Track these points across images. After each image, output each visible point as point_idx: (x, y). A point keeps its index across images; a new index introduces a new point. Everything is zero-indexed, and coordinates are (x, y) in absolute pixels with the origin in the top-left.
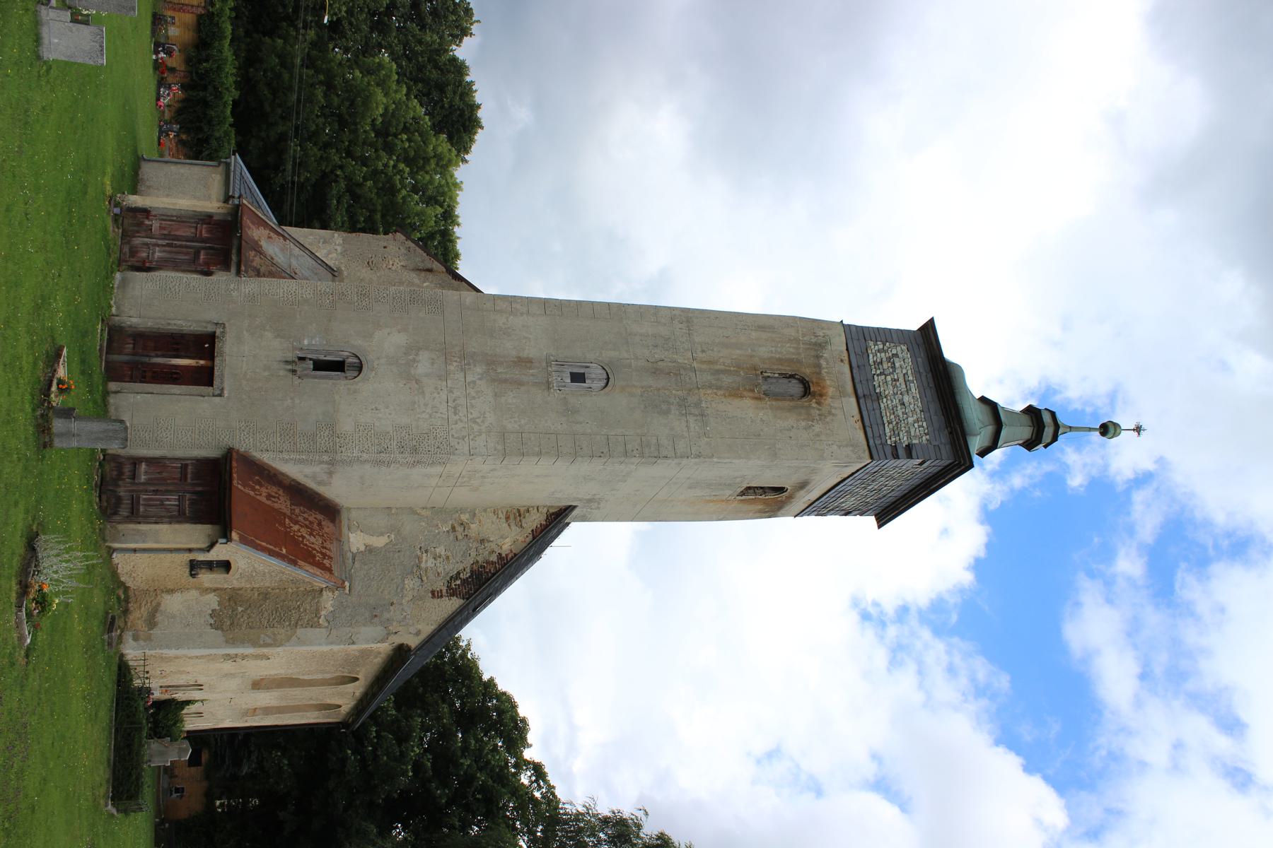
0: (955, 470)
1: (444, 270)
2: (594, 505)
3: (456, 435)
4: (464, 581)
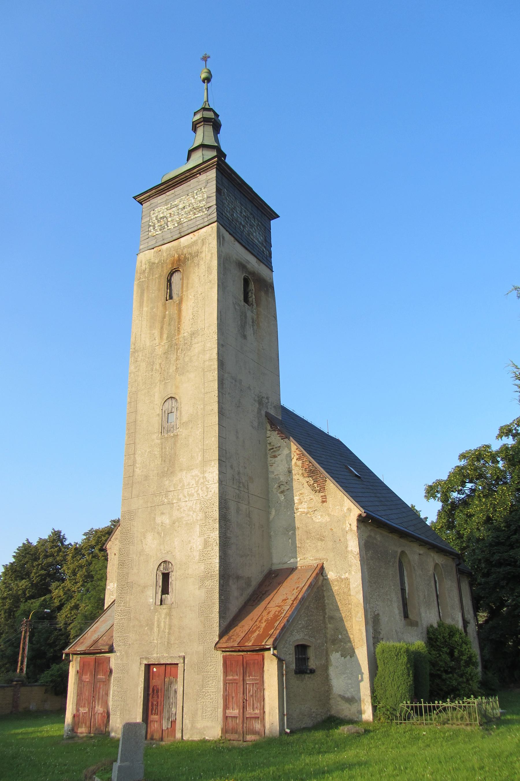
0: (223, 167)
2: (265, 400)
4: (315, 481)
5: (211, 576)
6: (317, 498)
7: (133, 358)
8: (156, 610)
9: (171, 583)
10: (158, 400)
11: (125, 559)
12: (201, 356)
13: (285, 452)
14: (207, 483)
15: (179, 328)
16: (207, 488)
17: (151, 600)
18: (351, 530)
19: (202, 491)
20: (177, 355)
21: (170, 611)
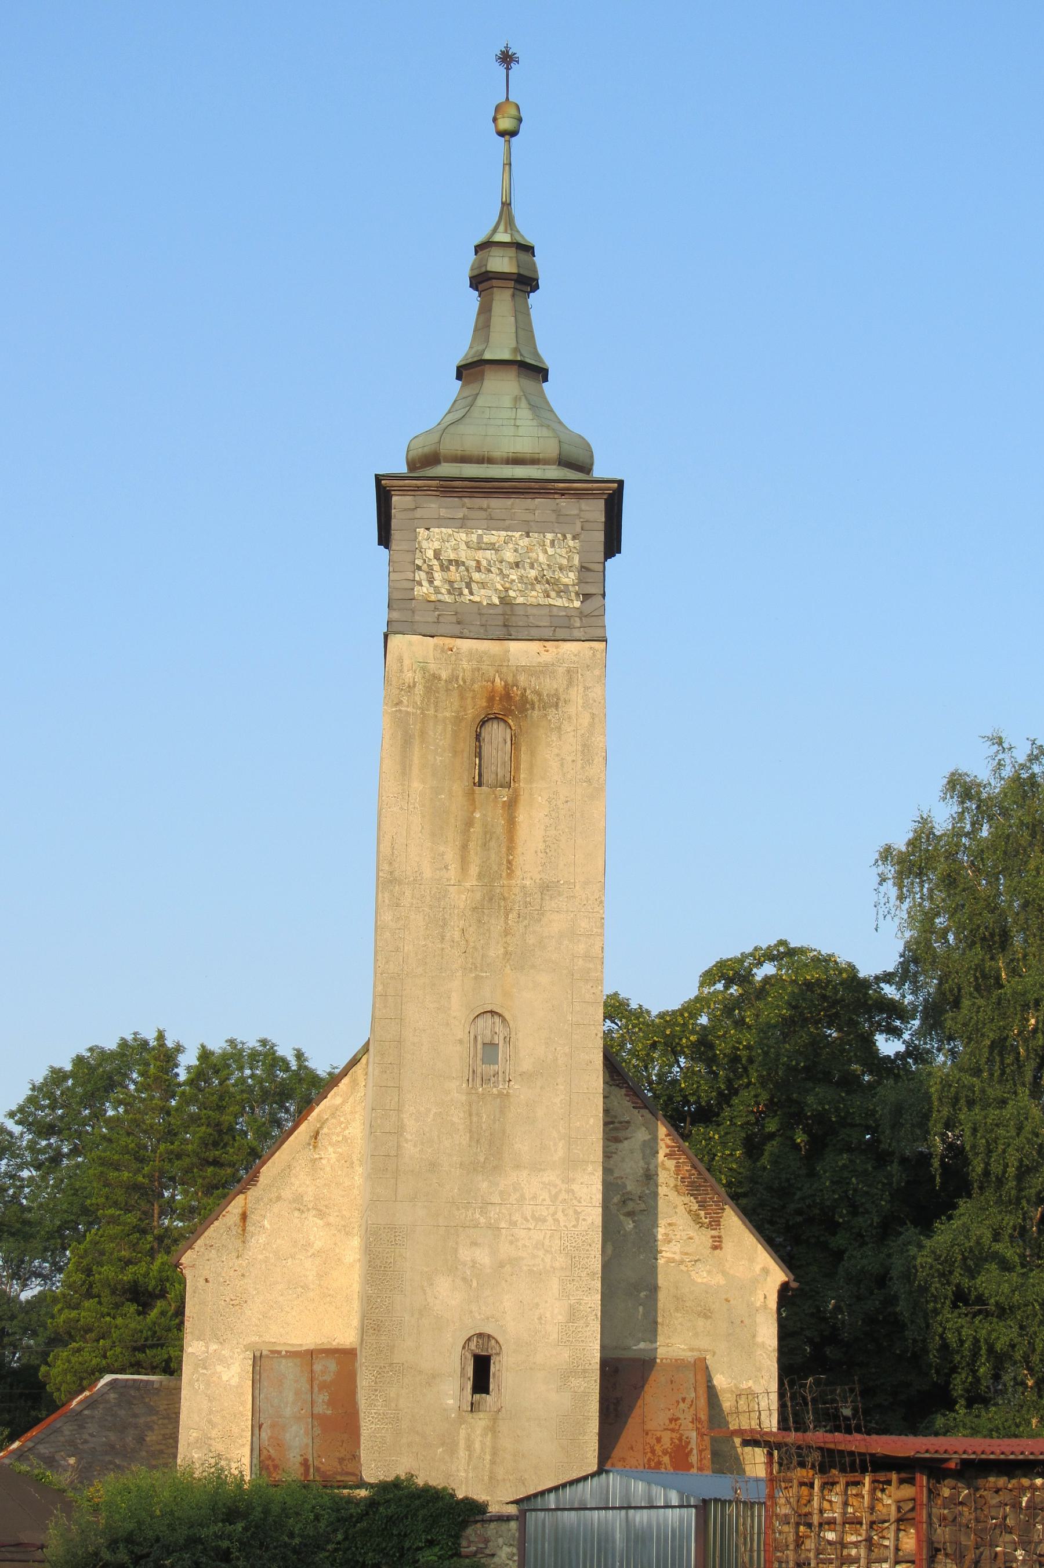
1: (241, 1197)
3: (574, 1223)
4: (702, 1205)
5: (585, 1371)
6: (703, 1238)
7: (386, 895)
8: (461, 1420)
9: (494, 1374)
10: (458, 1010)
11: (383, 1319)
12: (566, 942)
13: (641, 1135)
14: (575, 1202)
15: (509, 862)
16: (576, 1212)
17: (451, 1402)
18: (765, 1307)
19: (566, 1215)
20: (506, 923)
21: (494, 1423)
